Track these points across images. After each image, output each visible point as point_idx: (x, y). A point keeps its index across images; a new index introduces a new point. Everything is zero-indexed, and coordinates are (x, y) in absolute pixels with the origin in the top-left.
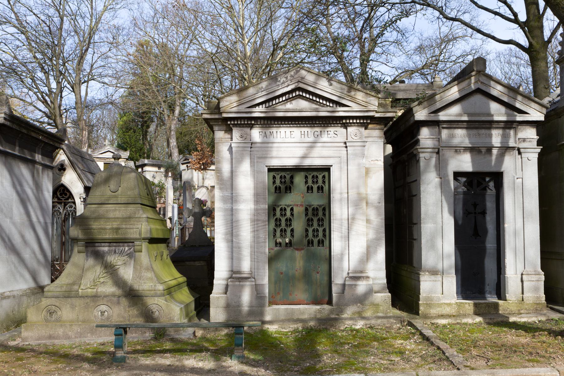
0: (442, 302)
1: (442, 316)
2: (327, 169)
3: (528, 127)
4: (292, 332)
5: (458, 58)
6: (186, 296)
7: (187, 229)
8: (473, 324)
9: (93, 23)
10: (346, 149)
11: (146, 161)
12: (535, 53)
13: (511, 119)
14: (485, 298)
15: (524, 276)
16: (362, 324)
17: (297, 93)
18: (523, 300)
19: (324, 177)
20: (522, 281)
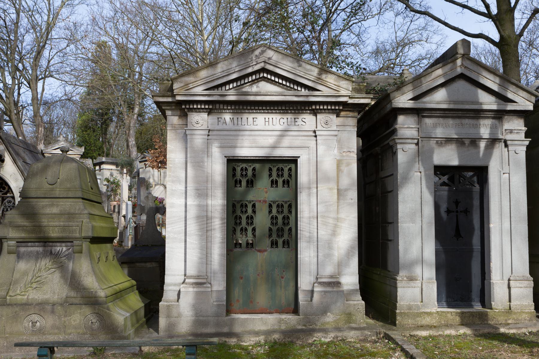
0: (421, 311)
1: (422, 327)
2: (294, 161)
3: (515, 117)
4: (252, 346)
5: (414, 62)
6: (135, 301)
7: (141, 228)
8: (458, 336)
9: (51, 19)
10: (315, 139)
11: (104, 159)
12: (506, 47)
13: (502, 108)
14: (471, 306)
15: (511, 282)
16: (333, 336)
17: (261, 75)
18: (510, 309)
19: (290, 169)
20: (509, 287)
